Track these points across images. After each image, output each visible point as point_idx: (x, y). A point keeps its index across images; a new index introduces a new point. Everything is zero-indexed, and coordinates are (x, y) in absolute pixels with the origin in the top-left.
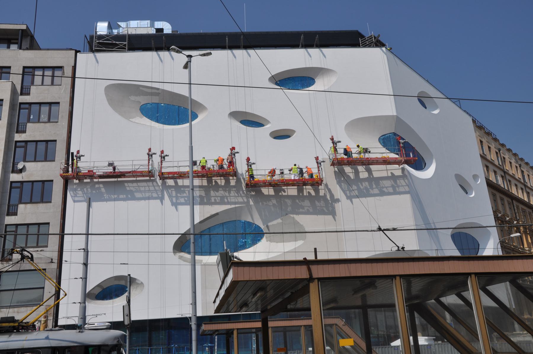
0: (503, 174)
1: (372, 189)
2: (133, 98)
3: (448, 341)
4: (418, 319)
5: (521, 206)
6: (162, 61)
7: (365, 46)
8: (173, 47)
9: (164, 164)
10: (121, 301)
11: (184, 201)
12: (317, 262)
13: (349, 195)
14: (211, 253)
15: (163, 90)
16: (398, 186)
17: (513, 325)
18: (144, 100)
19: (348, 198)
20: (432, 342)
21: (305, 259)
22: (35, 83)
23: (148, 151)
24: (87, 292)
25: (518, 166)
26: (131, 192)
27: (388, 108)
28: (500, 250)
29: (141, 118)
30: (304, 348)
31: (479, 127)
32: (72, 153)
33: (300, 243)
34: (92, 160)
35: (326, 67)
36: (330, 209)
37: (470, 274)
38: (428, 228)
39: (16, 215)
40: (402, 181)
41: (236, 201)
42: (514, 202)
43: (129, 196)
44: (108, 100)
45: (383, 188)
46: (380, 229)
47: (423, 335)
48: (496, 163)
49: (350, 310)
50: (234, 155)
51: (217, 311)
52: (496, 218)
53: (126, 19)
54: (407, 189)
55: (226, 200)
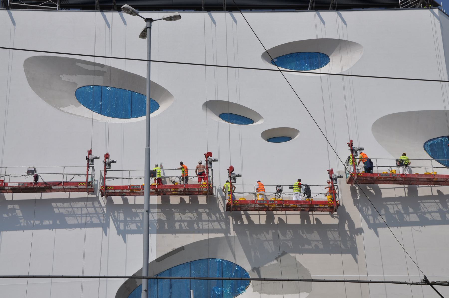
1: (408, 214)
2: (65, 77)
6: (109, 26)
8: (125, 5)
9: (109, 174)
11: (136, 228)
13: (372, 222)
15: (110, 68)
18: (81, 81)
19: (370, 226)
23: (87, 154)
26: (61, 217)
35: (346, 39)
36: (349, 244)
41: (211, 228)
43: (58, 222)
45: (425, 213)
46: (426, 282)
50: (211, 164)
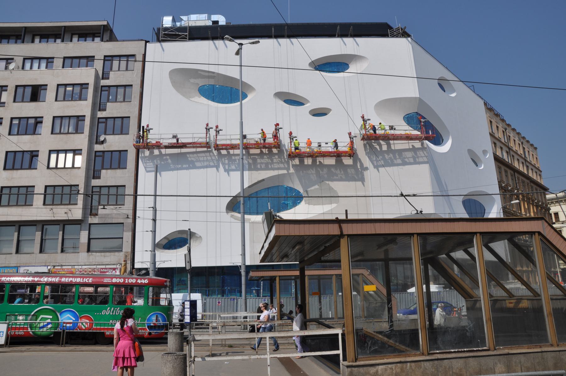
0: (508, 150)
1: (396, 159)
2: (192, 81)
3: (455, 288)
4: (431, 271)
5: (521, 177)
7: (393, 36)
9: (218, 137)
10: (183, 251)
12: (347, 221)
13: (376, 164)
14: (257, 213)
16: (418, 157)
17: (508, 274)
18: (201, 82)
20: (442, 290)
21: (337, 218)
22: (113, 69)
23: (205, 126)
24: (156, 242)
25: (520, 143)
26: (193, 162)
27: (411, 90)
28: (502, 214)
29: (200, 97)
30: (334, 292)
31: (490, 109)
32: (143, 127)
33: (334, 205)
34: (160, 132)
37: (476, 233)
38: (442, 193)
39: (100, 178)
40: (421, 152)
42: (516, 174)
44: (172, 83)
46: (402, 195)
47: (435, 284)
48: (503, 140)
49: (375, 263)
51: (262, 261)
52: (501, 187)
53: (187, 14)
54: (425, 159)
55: (270, 167)
